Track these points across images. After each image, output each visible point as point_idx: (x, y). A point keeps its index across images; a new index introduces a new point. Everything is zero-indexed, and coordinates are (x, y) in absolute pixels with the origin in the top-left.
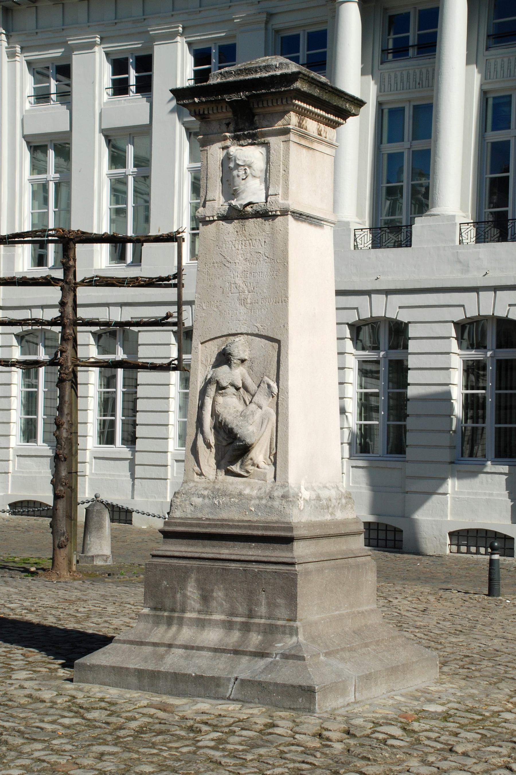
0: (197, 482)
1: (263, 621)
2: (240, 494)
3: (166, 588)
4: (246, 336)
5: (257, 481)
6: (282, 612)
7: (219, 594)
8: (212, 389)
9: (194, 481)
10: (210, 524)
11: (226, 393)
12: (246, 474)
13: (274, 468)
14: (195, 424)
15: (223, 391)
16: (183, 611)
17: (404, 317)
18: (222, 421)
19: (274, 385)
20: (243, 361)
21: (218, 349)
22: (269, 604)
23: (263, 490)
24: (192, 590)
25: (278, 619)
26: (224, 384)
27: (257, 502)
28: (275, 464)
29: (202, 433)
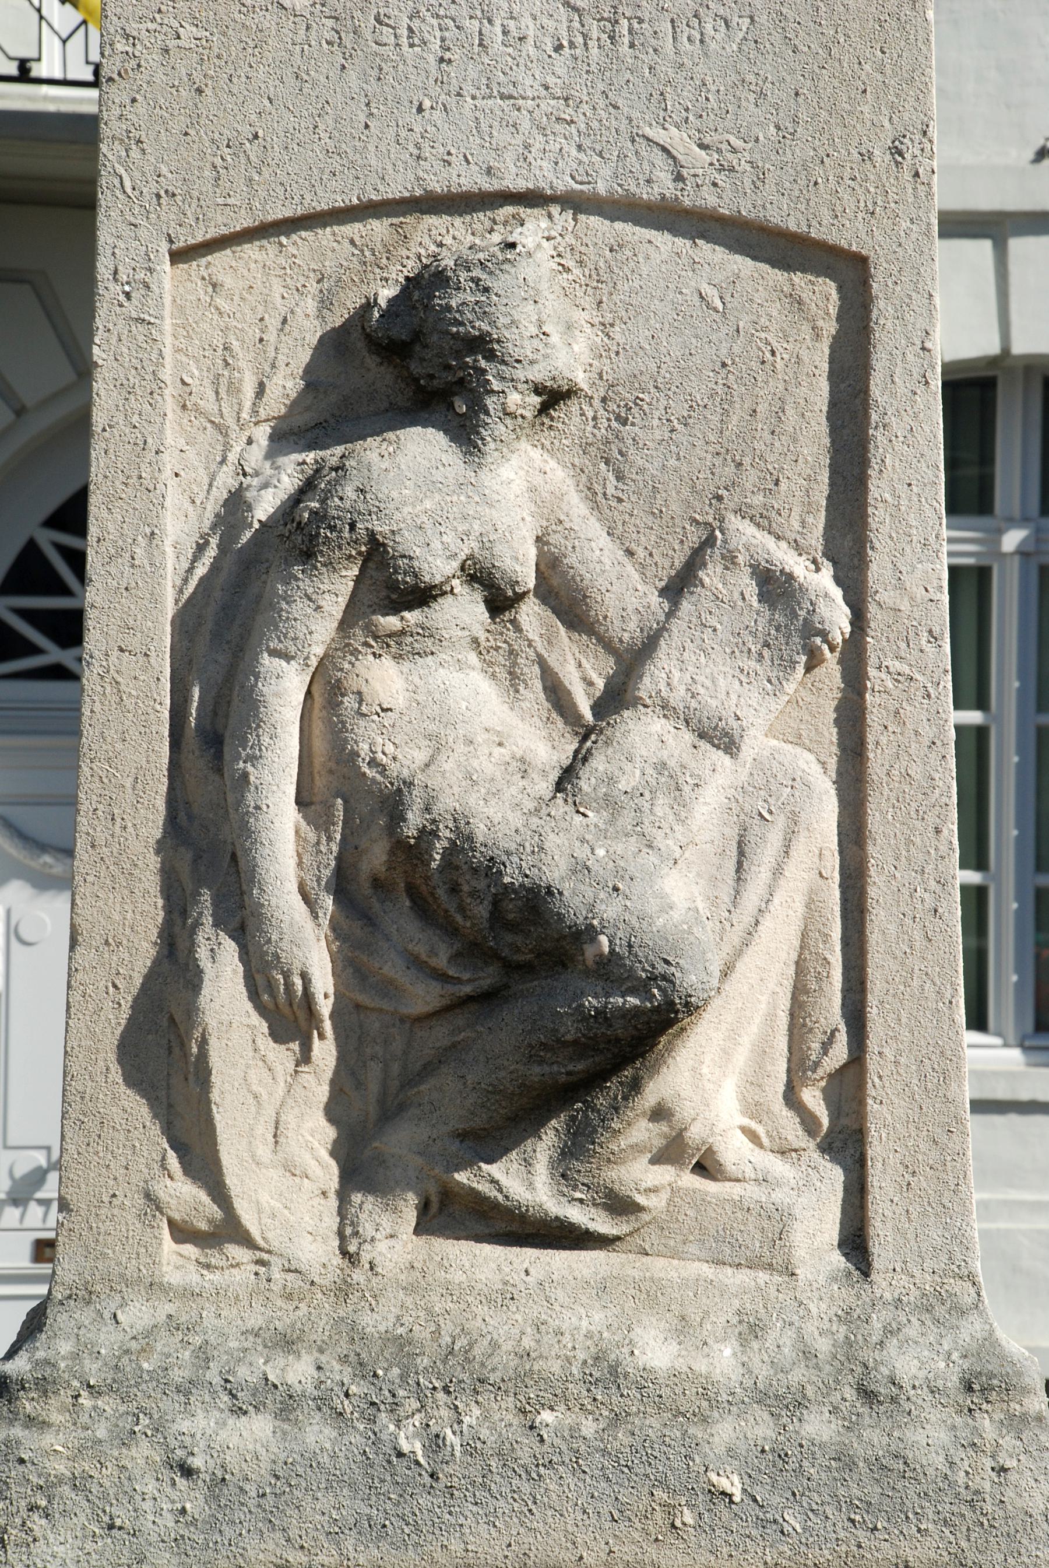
0: (189, 1294)
2: (607, 1373)
4: (564, 219)
5: (707, 1270)
8: (318, 606)
9: (155, 1287)
11: (426, 631)
12: (602, 1224)
13: (835, 1176)
14: (154, 862)
15: (412, 617)
18: (428, 834)
19: (821, 583)
20: (553, 397)
21: (325, 303)
23: (780, 1339)
26: (437, 565)
27: (762, 1429)
28: (846, 1144)
29: (243, 921)
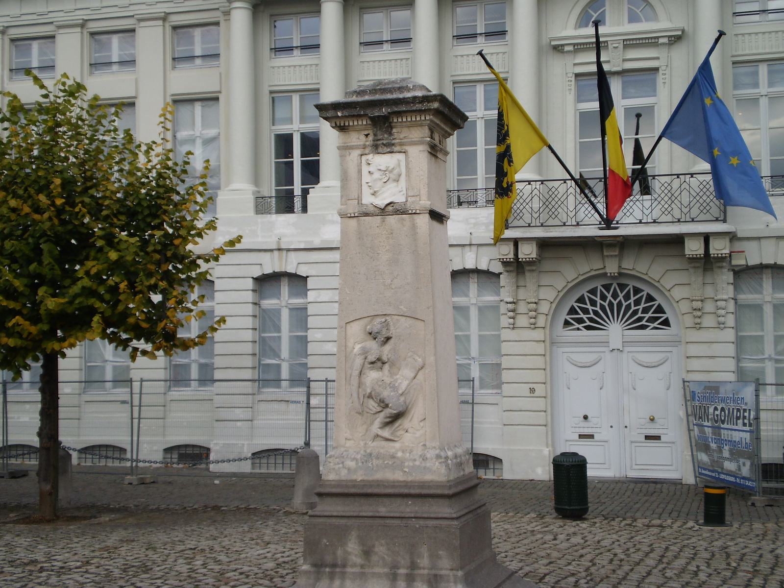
7: (381, 549)
16: (344, 566)
24: (353, 547)
25: (441, 569)
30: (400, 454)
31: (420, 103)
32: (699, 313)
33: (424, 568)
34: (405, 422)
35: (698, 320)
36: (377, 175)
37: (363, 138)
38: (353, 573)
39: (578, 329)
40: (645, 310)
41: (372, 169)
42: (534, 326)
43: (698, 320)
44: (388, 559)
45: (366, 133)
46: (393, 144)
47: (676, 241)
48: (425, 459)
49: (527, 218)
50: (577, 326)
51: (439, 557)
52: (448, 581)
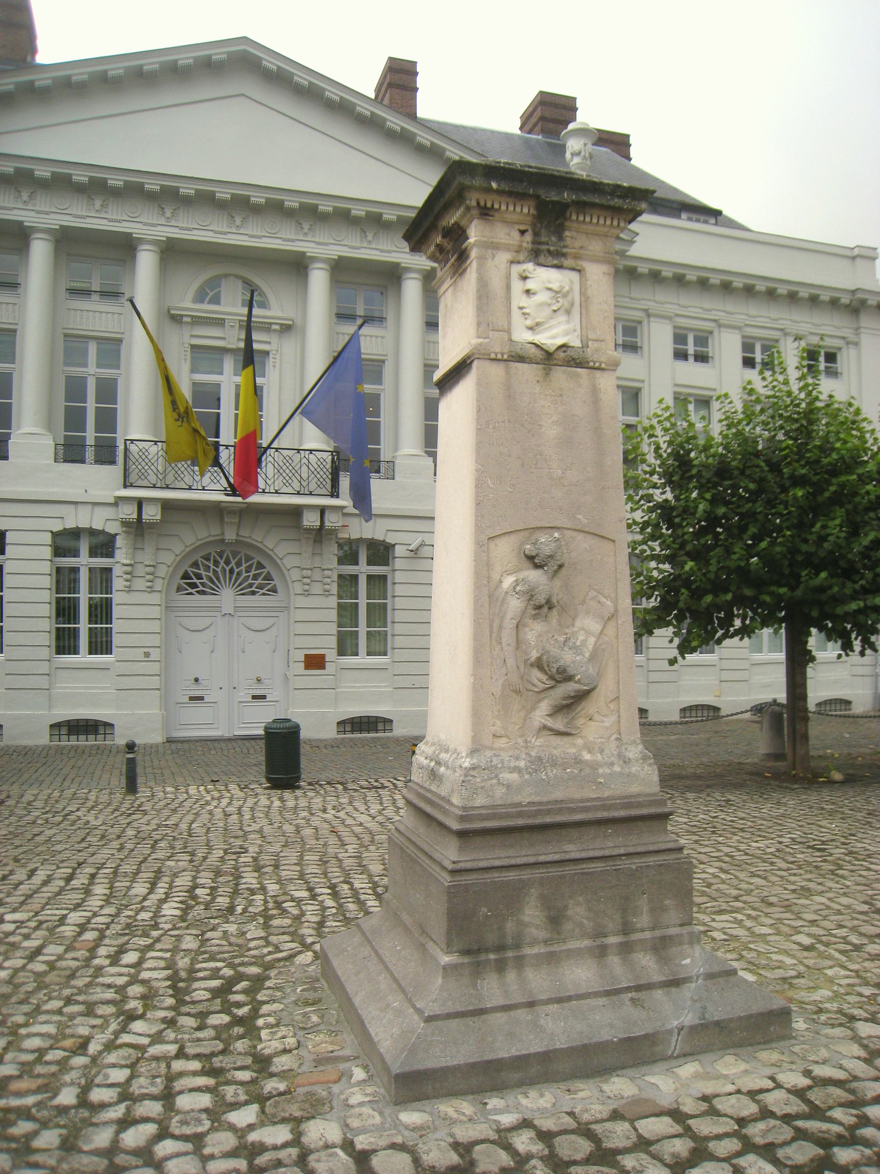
1: (647, 935)
3: (487, 917)
6: (673, 916)
7: (577, 910)
10: (539, 810)
16: (517, 946)
17: (391, 539)
22: (652, 910)
24: (532, 913)
30: (587, 757)
31: (619, 197)
32: (308, 581)
33: (643, 931)
34: (590, 706)
35: (306, 587)
36: (543, 297)
37: (516, 235)
38: (537, 955)
39: (191, 594)
40: (255, 577)
41: (530, 285)
42: (151, 590)
43: (306, 587)
44: (589, 925)
45: (522, 228)
46: (564, 255)
47: (296, 512)
48: (627, 762)
49: (153, 478)
50: (191, 590)
51: (664, 909)
52: (681, 943)
